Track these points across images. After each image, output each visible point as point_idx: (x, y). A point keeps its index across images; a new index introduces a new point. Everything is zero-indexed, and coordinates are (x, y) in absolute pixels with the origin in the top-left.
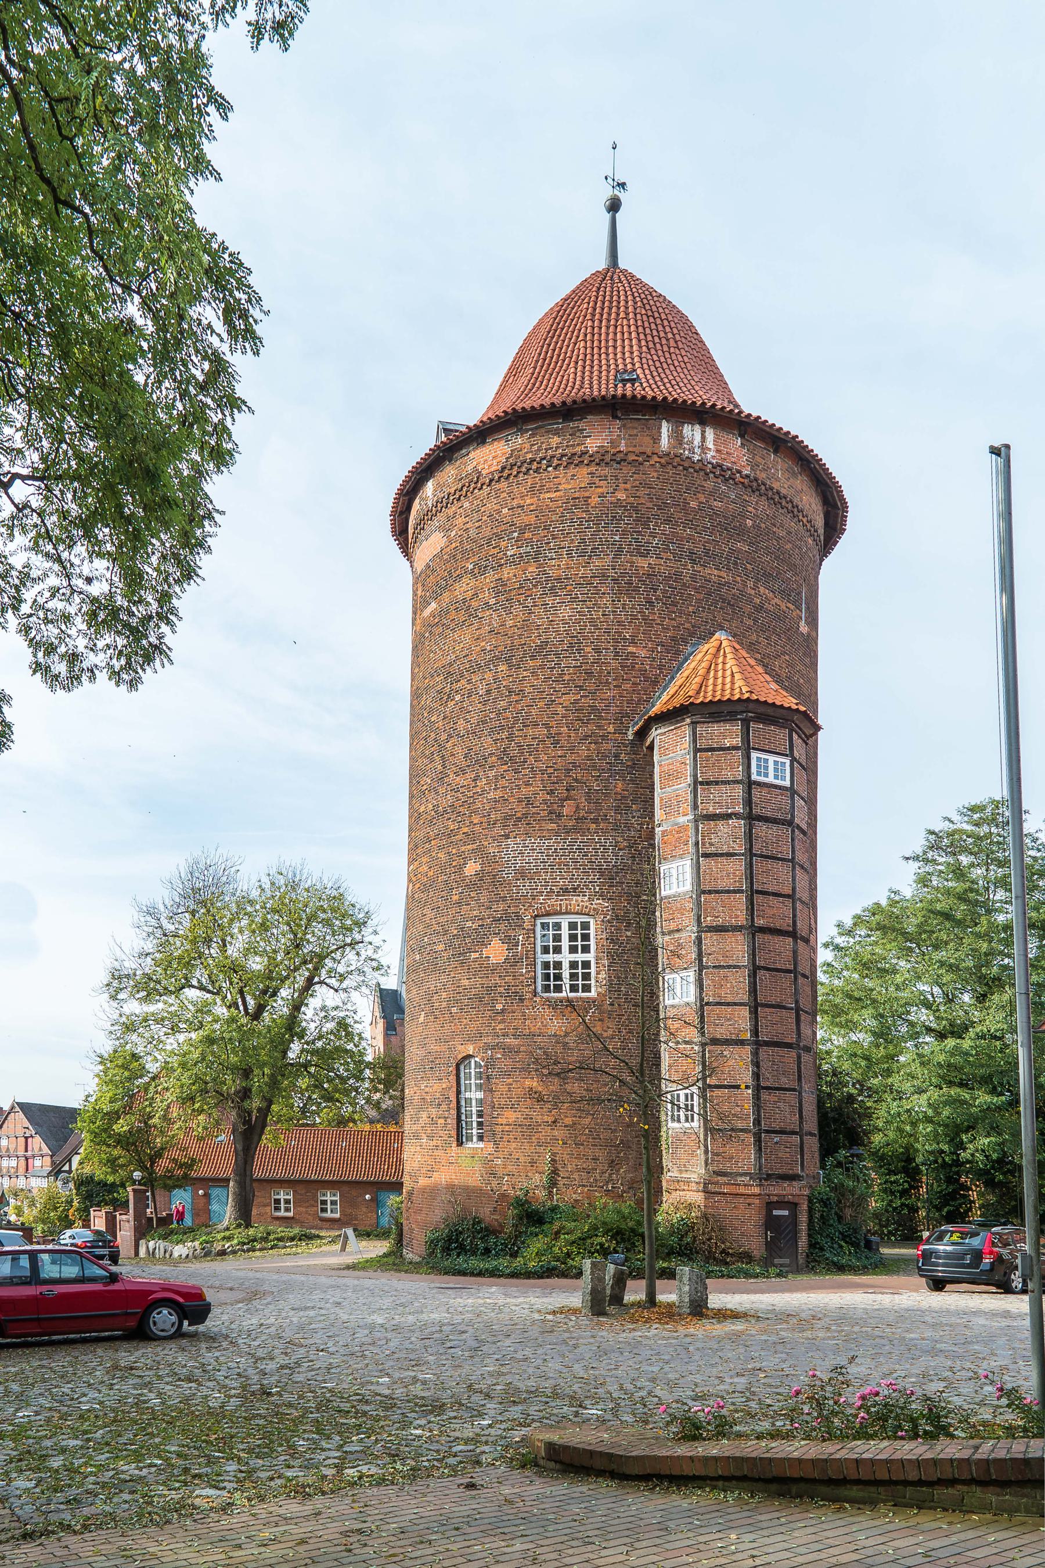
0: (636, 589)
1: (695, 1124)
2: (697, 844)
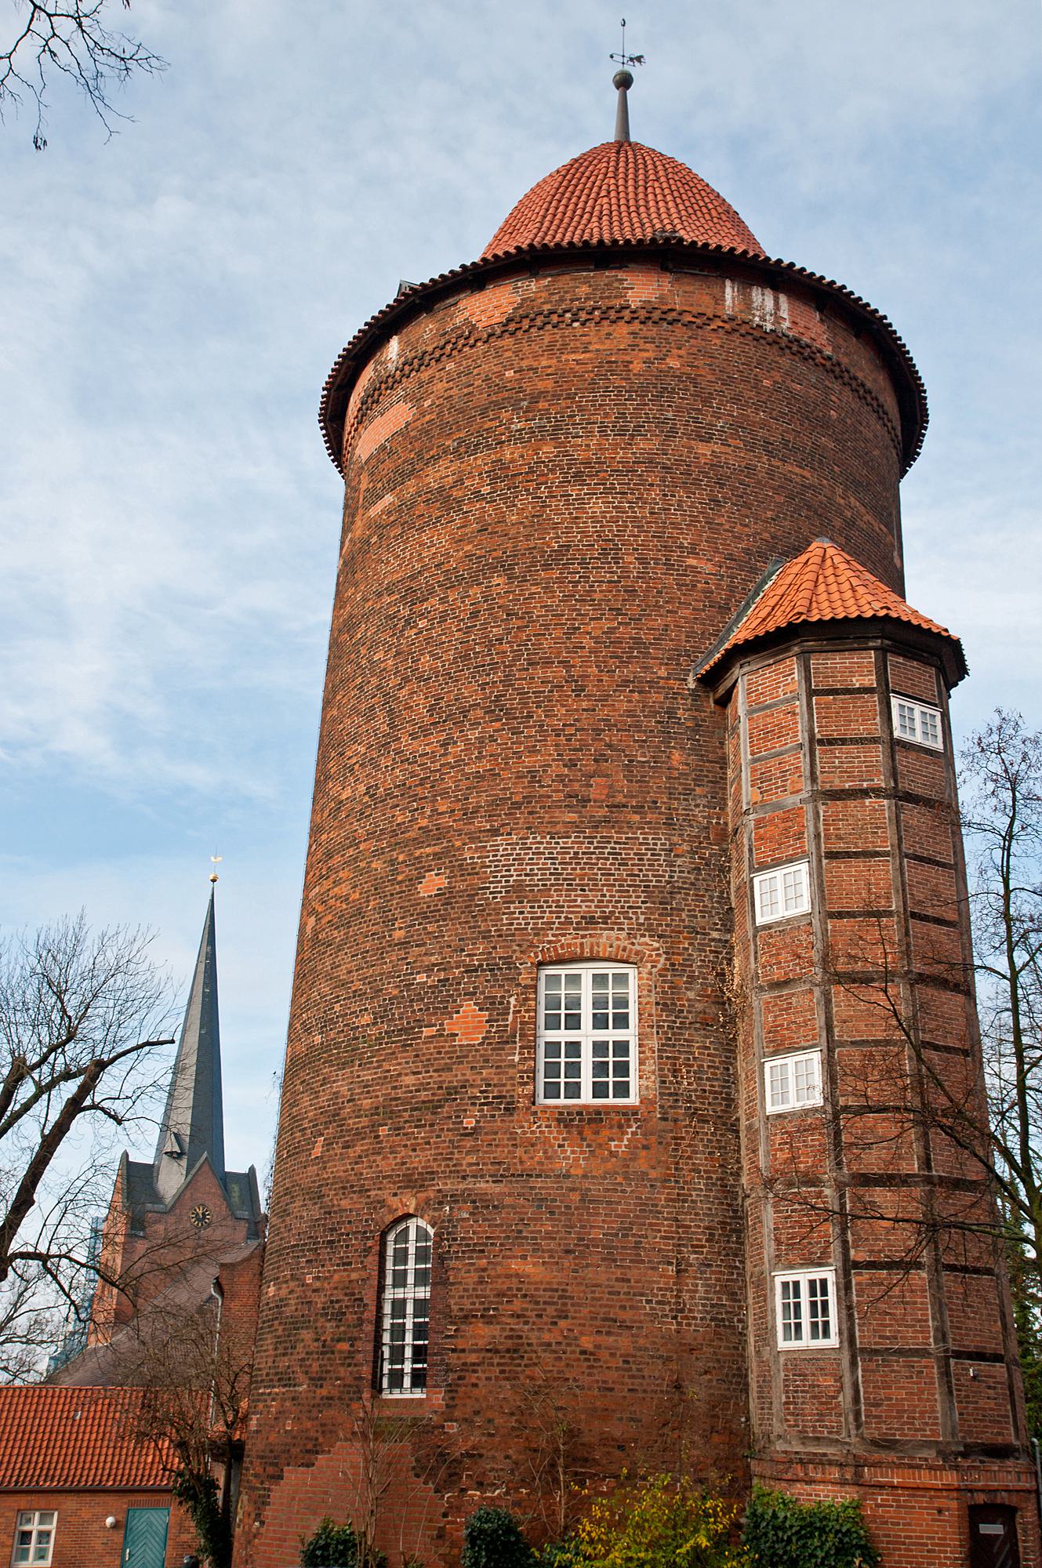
0: (696, 482)
1: (833, 1341)
2: (817, 836)
